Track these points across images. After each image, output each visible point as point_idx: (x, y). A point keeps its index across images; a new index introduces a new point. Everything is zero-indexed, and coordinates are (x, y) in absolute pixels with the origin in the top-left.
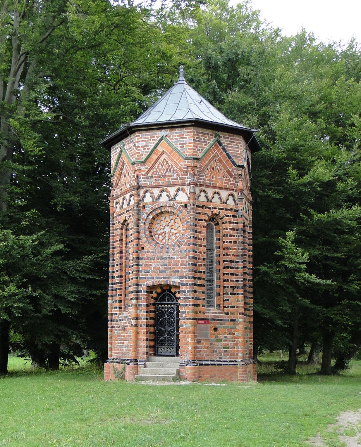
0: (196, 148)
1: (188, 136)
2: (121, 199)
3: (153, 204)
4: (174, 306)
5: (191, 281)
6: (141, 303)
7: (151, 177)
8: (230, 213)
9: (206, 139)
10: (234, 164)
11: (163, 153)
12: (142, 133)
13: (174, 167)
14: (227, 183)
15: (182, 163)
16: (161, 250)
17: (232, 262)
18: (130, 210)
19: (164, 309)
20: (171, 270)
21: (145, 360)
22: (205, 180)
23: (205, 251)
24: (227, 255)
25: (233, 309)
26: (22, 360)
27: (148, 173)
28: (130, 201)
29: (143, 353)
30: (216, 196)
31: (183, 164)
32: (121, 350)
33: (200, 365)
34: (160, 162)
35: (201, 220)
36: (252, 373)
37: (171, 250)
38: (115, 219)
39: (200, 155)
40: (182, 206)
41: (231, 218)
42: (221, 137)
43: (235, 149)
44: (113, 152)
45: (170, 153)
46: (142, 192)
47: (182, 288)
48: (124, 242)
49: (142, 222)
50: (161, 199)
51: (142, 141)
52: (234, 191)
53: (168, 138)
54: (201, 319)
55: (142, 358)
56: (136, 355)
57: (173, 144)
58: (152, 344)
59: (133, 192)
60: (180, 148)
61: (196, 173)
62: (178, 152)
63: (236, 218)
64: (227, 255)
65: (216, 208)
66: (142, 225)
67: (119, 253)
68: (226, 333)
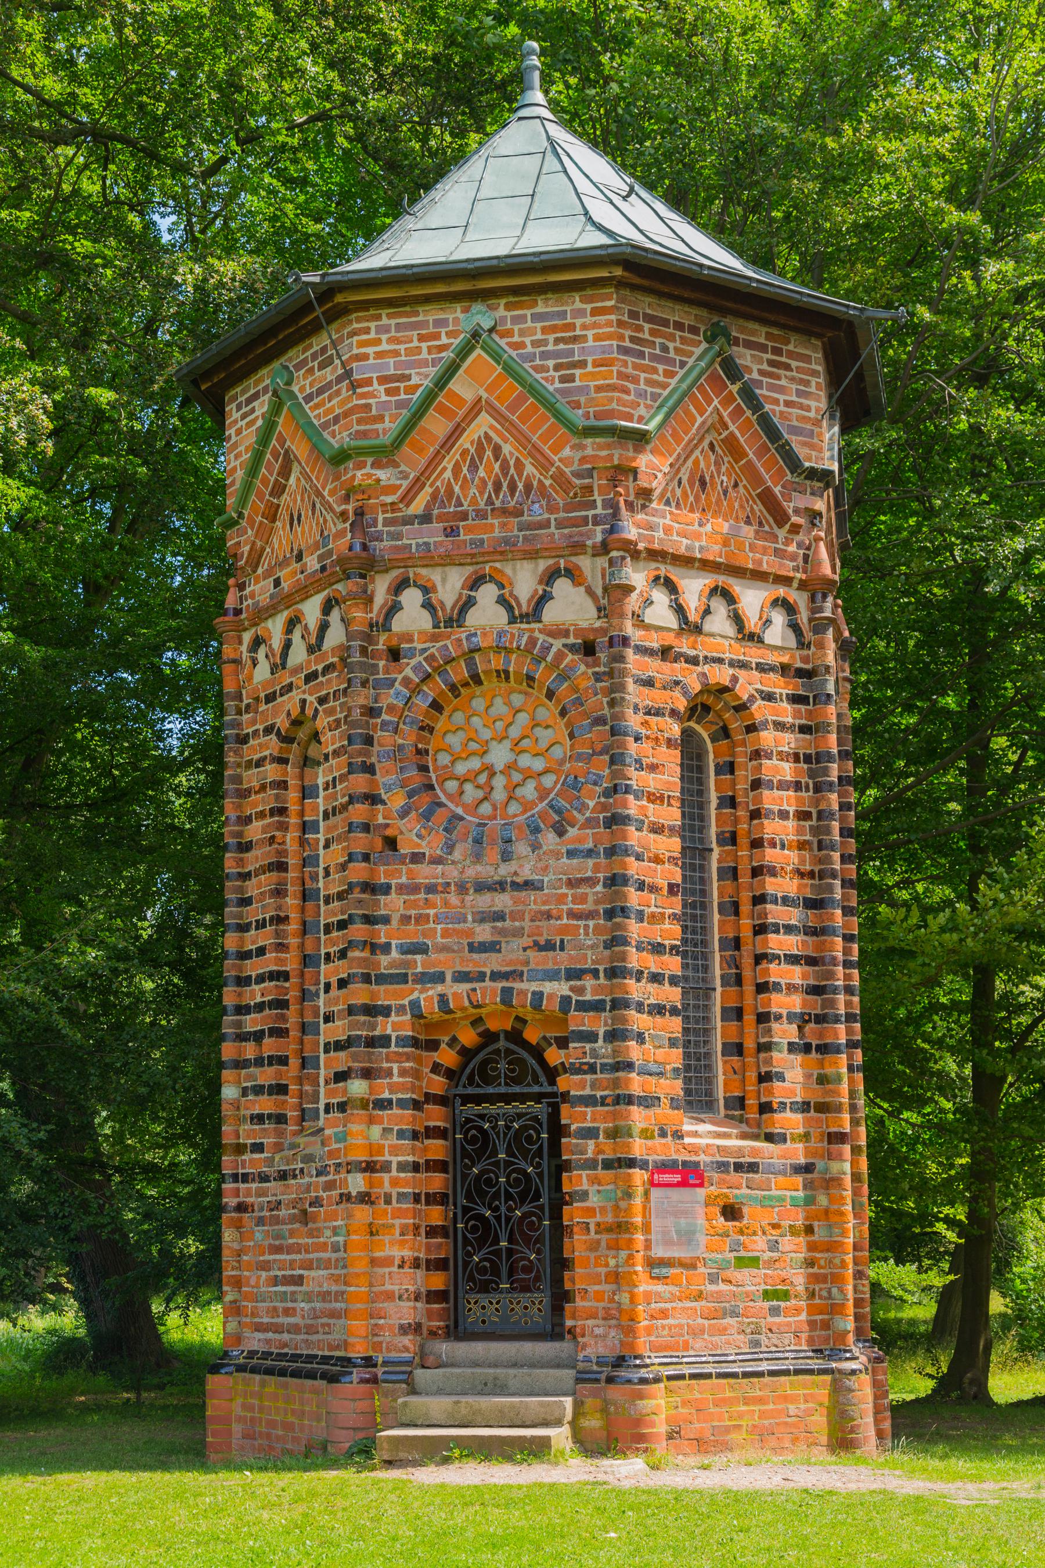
1: (595, 326)
2: (275, 627)
3: (434, 638)
4: (539, 1109)
6: (386, 1095)
7: (426, 518)
9: (671, 345)
10: (793, 462)
11: (477, 407)
12: (378, 317)
13: (529, 469)
15: (567, 452)
18: (327, 669)
19: (494, 1119)
20: (527, 941)
23: (676, 855)
26: (192, 1336)
27: (408, 498)
28: (324, 627)
34: (466, 452)
38: (246, 717)
40: (572, 648)
42: (736, 342)
43: (794, 398)
44: (236, 415)
46: (381, 587)
48: (293, 820)
50: (474, 618)
51: (379, 355)
52: (795, 584)
53: (503, 342)
57: (526, 365)
58: (438, 1281)
59: (339, 586)
60: (557, 385)
63: (803, 708)
65: (720, 661)
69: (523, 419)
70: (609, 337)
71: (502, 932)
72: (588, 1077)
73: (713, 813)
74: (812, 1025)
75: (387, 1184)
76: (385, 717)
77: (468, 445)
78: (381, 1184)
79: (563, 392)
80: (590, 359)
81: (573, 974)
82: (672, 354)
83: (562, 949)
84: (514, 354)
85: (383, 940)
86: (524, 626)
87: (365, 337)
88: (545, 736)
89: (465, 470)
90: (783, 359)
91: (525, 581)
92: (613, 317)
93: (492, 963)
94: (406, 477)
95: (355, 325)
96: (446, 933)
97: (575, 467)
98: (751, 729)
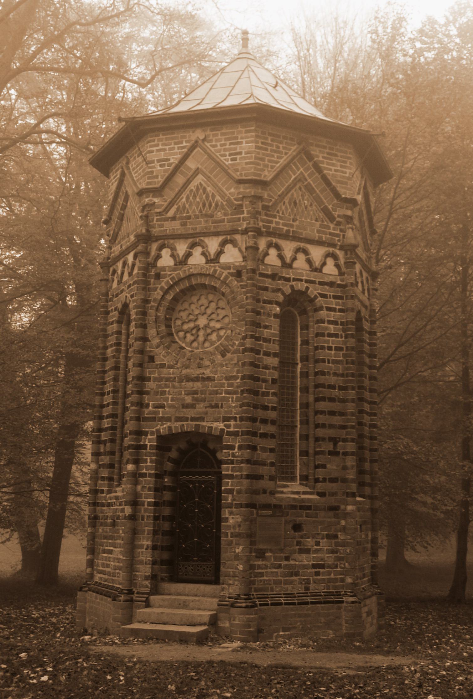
0: (261, 162)
2: (120, 264)
3: (175, 270)
5: (246, 426)
6: (144, 471)
7: (173, 218)
8: (327, 290)
9: (281, 146)
10: (337, 195)
11: (197, 172)
12: (158, 136)
13: (218, 198)
14: (324, 233)
15: (232, 190)
20: (207, 404)
22: (277, 223)
24: (323, 373)
25: (334, 485)
27: (167, 210)
29: (146, 576)
30: (301, 257)
31: (232, 192)
32: (108, 566)
33: (261, 605)
34: (192, 190)
35: (270, 302)
36: (375, 614)
37: (207, 363)
38: (110, 303)
39: (268, 175)
40: (232, 274)
41: (332, 299)
42: (312, 144)
43: (339, 168)
45: (211, 172)
46: (154, 246)
47: (227, 440)
49: (152, 306)
50: (191, 261)
51: (158, 151)
52: (338, 247)
53: (208, 145)
54: (267, 506)
56: (131, 579)
57: (218, 154)
58: (166, 556)
60: (230, 162)
63: (340, 301)
64: (323, 373)
65: (301, 280)
66: (152, 312)
69: (215, 176)
70: (251, 142)
72: (230, 466)
73: (299, 347)
74: (341, 443)
75: (142, 511)
76: (152, 304)
77: (193, 188)
78: (140, 512)
79: (232, 165)
80: (243, 152)
81: (226, 419)
82: (281, 149)
83: (222, 407)
84: (212, 149)
87: (153, 143)
88: (222, 313)
89: (191, 198)
90: (334, 152)
91: (213, 245)
92: (254, 134)
93: (190, 413)
94: (166, 201)
95: (149, 139)
96: (173, 400)
98: (316, 310)
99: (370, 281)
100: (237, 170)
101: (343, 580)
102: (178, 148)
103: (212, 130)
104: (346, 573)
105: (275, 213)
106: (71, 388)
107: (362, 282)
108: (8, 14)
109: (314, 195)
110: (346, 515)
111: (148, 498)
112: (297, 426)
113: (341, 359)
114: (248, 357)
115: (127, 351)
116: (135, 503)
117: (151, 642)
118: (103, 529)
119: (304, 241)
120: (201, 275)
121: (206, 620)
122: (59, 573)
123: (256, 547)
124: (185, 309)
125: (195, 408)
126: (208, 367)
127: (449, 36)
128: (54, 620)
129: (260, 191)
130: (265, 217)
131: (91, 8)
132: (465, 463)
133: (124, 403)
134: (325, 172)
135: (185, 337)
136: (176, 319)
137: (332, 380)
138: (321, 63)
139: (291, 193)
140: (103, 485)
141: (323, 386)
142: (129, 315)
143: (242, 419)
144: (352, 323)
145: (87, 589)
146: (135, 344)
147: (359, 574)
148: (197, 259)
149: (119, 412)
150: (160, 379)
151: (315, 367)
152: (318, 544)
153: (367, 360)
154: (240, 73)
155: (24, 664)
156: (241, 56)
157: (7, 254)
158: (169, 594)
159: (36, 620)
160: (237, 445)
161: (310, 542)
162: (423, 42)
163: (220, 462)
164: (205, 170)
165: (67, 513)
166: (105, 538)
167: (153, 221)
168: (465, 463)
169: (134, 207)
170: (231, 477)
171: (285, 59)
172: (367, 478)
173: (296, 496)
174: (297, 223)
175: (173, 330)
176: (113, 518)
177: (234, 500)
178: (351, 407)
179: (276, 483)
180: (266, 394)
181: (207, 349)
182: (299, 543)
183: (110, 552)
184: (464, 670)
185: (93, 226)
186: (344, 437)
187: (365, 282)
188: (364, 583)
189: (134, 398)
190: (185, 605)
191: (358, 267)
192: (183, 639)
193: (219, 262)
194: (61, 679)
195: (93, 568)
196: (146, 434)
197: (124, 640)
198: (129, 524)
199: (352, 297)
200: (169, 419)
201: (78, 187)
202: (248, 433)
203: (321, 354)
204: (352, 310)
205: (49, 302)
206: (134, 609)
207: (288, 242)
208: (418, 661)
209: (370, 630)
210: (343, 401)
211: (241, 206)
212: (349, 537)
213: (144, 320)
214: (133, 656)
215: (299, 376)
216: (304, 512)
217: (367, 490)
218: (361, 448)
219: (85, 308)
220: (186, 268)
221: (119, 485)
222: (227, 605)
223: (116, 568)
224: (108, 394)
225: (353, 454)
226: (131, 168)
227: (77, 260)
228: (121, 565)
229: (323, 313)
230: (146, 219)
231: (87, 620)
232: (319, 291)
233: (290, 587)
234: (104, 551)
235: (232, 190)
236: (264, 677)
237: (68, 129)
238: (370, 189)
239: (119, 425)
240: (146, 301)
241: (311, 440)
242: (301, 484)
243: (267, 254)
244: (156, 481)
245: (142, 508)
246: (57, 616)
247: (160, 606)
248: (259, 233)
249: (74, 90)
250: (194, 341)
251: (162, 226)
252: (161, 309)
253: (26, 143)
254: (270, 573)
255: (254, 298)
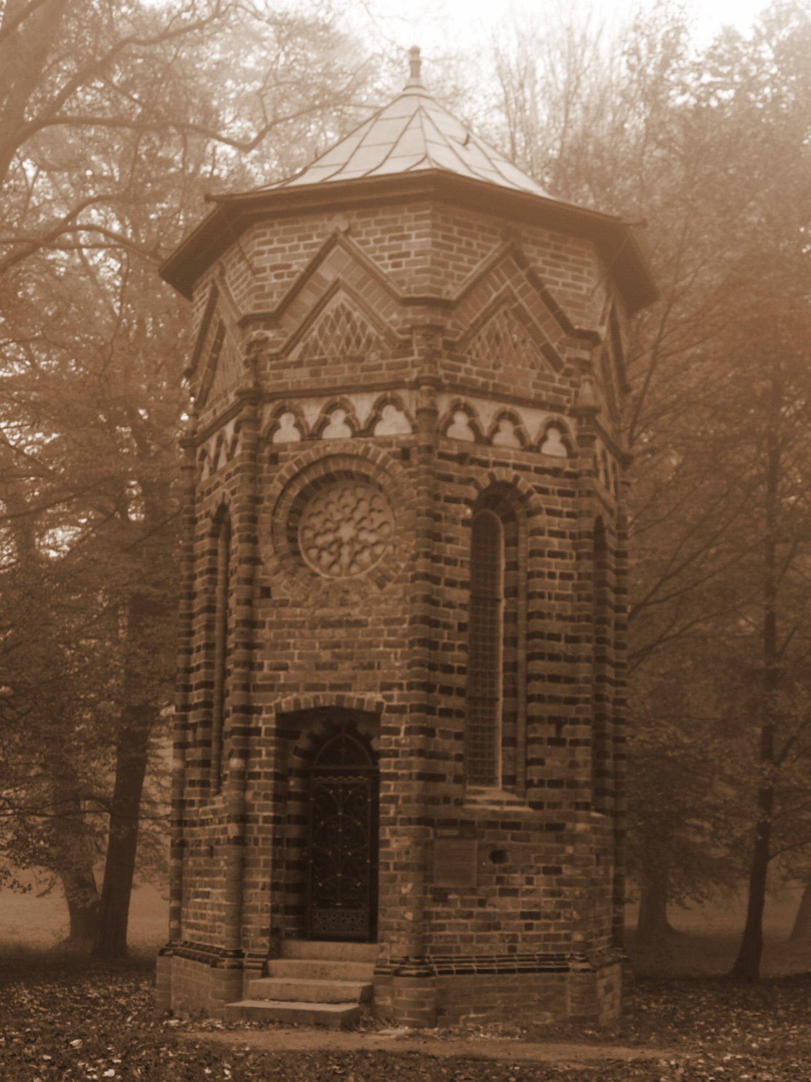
0: (442, 270)
2: (213, 442)
5: (417, 697)
6: (257, 769)
7: (298, 364)
8: (548, 482)
9: (475, 242)
10: (566, 325)
11: (336, 286)
12: (272, 225)
13: (371, 329)
14: (544, 388)
15: (395, 316)
16: (324, 597)
17: (556, 637)
20: (354, 663)
21: (265, 951)
22: (468, 371)
24: (540, 615)
25: (556, 791)
27: (288, 349)
29: (262, 930)
30: (507, 428)
31: (394, 318)
32: (203, 916)
33: (441, 973)
34: (327, 318)
35: (456, 500)
36: (617, 991)
37: (355, 598)
38: (198, 506)
39: (453, 291)
40: (394, 455)
41: (556, 497)
43: (569, 281)
45: (359, 286)
46: (268, 411)
47: (388, 720)
49: (265, 508)
50: (329, 433)
51: (272, 251)
52: (567, 412)
53: (354, 240)
54: (450, 823)
55: (261, 944)
56: (239, 935)
57: (370, 256)
58: (293, 899)
60: (390, 269)
61: (440, 348)
62: (381, 282)
63: (570, 500)
64: (540, 615)
65: (506, 465)
66: (265, 517)
67: (203, 610)
68: (531, 867)
70: (426, 235)
71: (338, 657)
77: (329, 313)
79: (395, 274)
80: (413, 252)
82: (475, 248)
84: (362, 248)
85: (259, 660)
86: (362, 439)
87: (263, 239)
88: (378, 518)
89: (327, 330)
90: (563, 254)
91: (363, 406)
92: (429, 222)
93: (328, 677)
94: (286, 336)
96: (300, 656)
97: (400, 327)
98: (531, 514)
99: (618, 470)
100: (401, 283)
101: (568, 937)
102: (306, 247)
103: (360, 216)
104: (573, 926)
105: (465, 355)
106: (139, 647)
107: (606, 471)
108: (15, 24)
109: (529, 325)
110: (574, 838)
111: (263, 811)
112: (497, 700)
113: (570, 592)
114: (422, 588)
115: (227, 582)
116: (243, 818)
117: (271, 1026)
118: (194, 862)
119: (511, 401)
120: (343, 456)
121: (357, 994)
122: (128, 943)
123: (433, 885)
124: (319, 513)
125: (336, 669)
126: (356, 604)
127: (760, 62)
128: (122, 1001)
129: (440, 317)
130: (447, 361)
131: (155, 16)
132: (764, 766)
133: (223, 665)
134: (548, 286)
135: (319, 558)
136: (305, 528)
137: (555, 626)
138: (544, 116)
139: (490, 321)
140: (193, 794)
141: (540, 635)
142: (229, 524)
143: (410, 686)
144: (589, 535)
145: (171, 952)
146: (239, 569)
147: (595, 930)
148: (337, 430)
149: (216, 678)
150: (279, 625)
151: (527, 606)
152: (530, 881)
153: (612, 597)
154: (407, 120)
155: (78, 1055)
156: (408, 91)
157: (30, 438)
158: (299, 958)
159: (95, 1002)
160: (403, 728)
161: (518, 879)
162: (715, 73)
163: (377, 755)
164: (349, 284)
165: (139, 849)
166: (198, 873)
167: (265, 369)
168: (764, 766)
169: (234, 346)
170: (393, 777)
171: (484, 108)
172: (609, 783)
173: (497, 808)
174: (501, 371)
175: (301, 546)
176: (209, 842)
177: (398, 812)
178: (584, 670)
179: (465, 787)
180: (448, 647)
181: (355, 577)
182: (500, 880)
183: (207, 895)
184: (752, 1066)
185: (168, 389)
186: (573, 716)
187: (610, 470)
188: (602, 944)
189: (239, 654)
190: (323, 974)
191: (599, 445)
192: (321, 1022)
193: (372, 435)
194: (135, 1073)
195: (180, 922)
196: (259, 711)
197: (231, 1024)
198: (234, 850)
199: (589, 494)
200: (295, 688)
201: (141, 323)
202: (420, 708)
203: (538, 585)
204: (589, 514)
205: (100, 515)
206: (245, 980)
207: (486, 403)
208: (683, 1054)
209: (609, 1013)
210: (572, 660)
211: (408, 342)
212: (578, 872)
213: (254, 530)
214: (245, 1045)
215: (501, 618)
216: (509, 833)
217: (609, 802)
218: (600, 735)
219: (158, 523)
220: (319, 445)
221: (218, 793)
222: (389, 973)
223: (215, 919)
224: (199, 649)
225: (586, 743)
226: (228, 282)
227: (144, 447)
228: (224, 913)
229: (542, 520)
230: (254, 365)
231: (173, 999)
232: (536, 483)
233: (486, 946)
234: (197, 895)
235: (395, 316)
236: (444, 1071)
237: (124, 228)
238: (621, 318)
239: (215, 699)
240: (256, 500)
241: (521, 720)
242: (504, 789)
243: (450, 422)
244: (276, 785)
245: (255, 827)
246: (127, 996)
247: (285, 975)
248: (438, 387)
249: (130, 159)
250: (334, 563)
251: (280, 376)
252: (281, 512)
253: (53, 248)
254: (455, 925)
255: (429, 493)
